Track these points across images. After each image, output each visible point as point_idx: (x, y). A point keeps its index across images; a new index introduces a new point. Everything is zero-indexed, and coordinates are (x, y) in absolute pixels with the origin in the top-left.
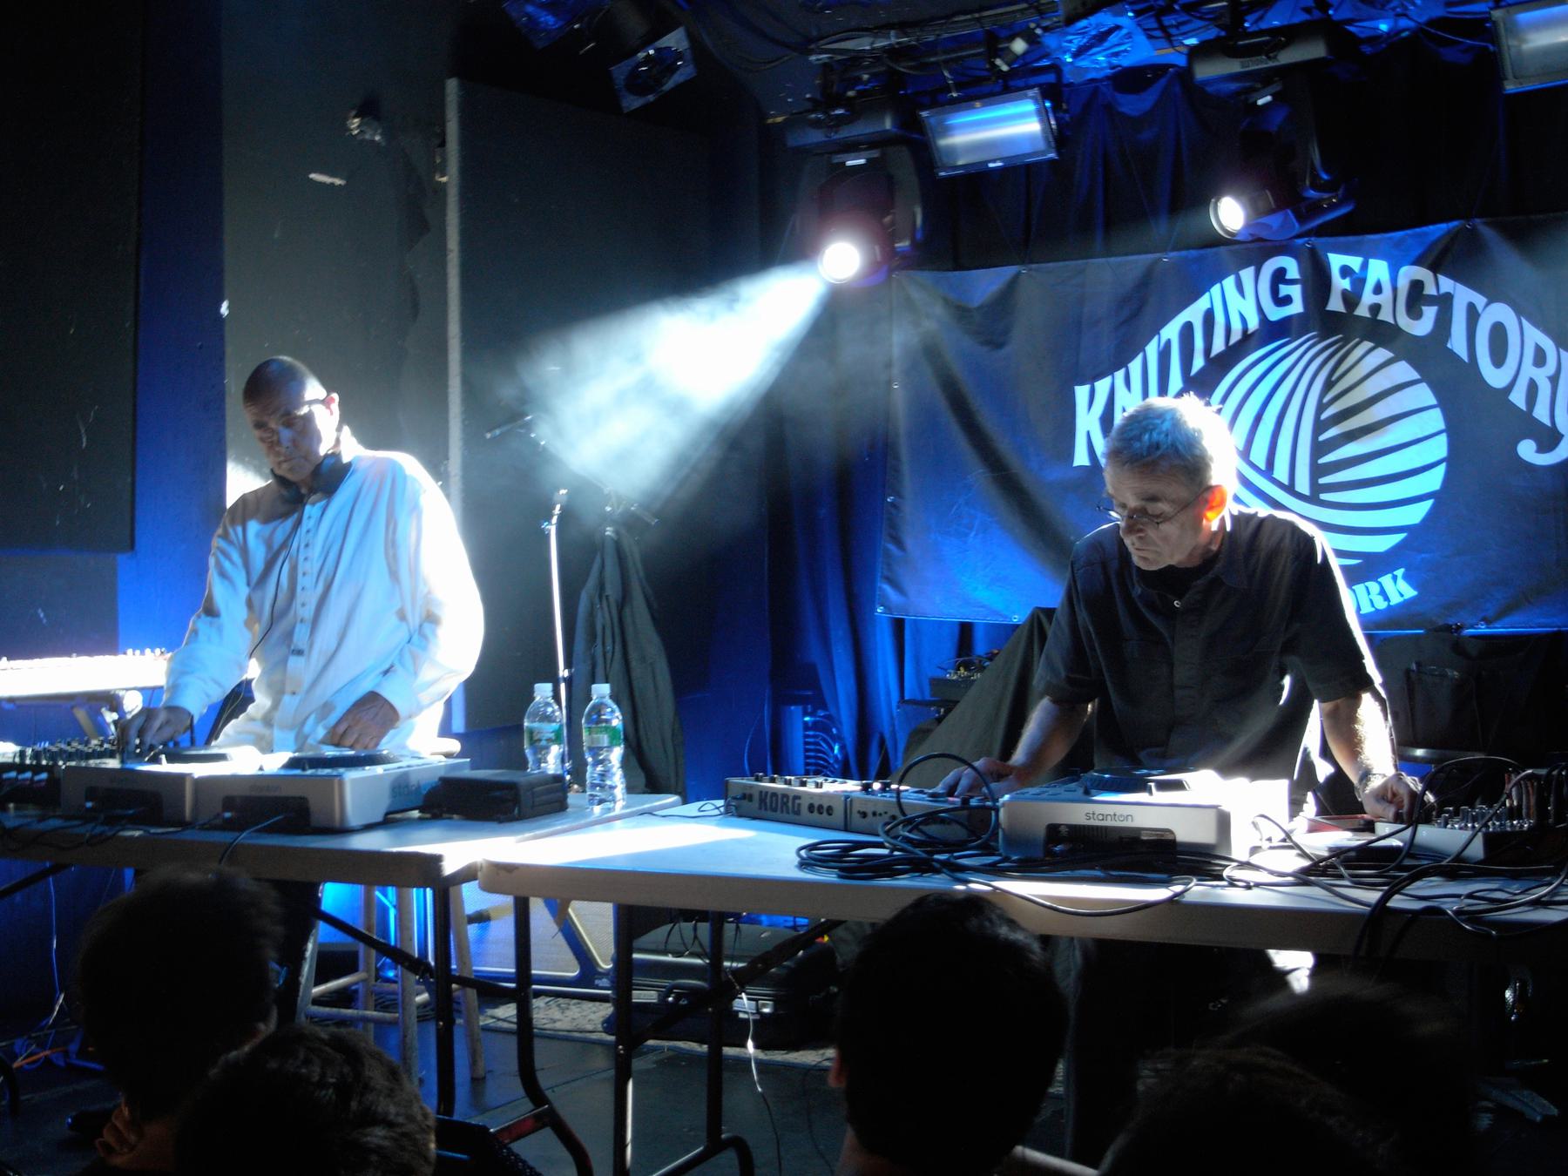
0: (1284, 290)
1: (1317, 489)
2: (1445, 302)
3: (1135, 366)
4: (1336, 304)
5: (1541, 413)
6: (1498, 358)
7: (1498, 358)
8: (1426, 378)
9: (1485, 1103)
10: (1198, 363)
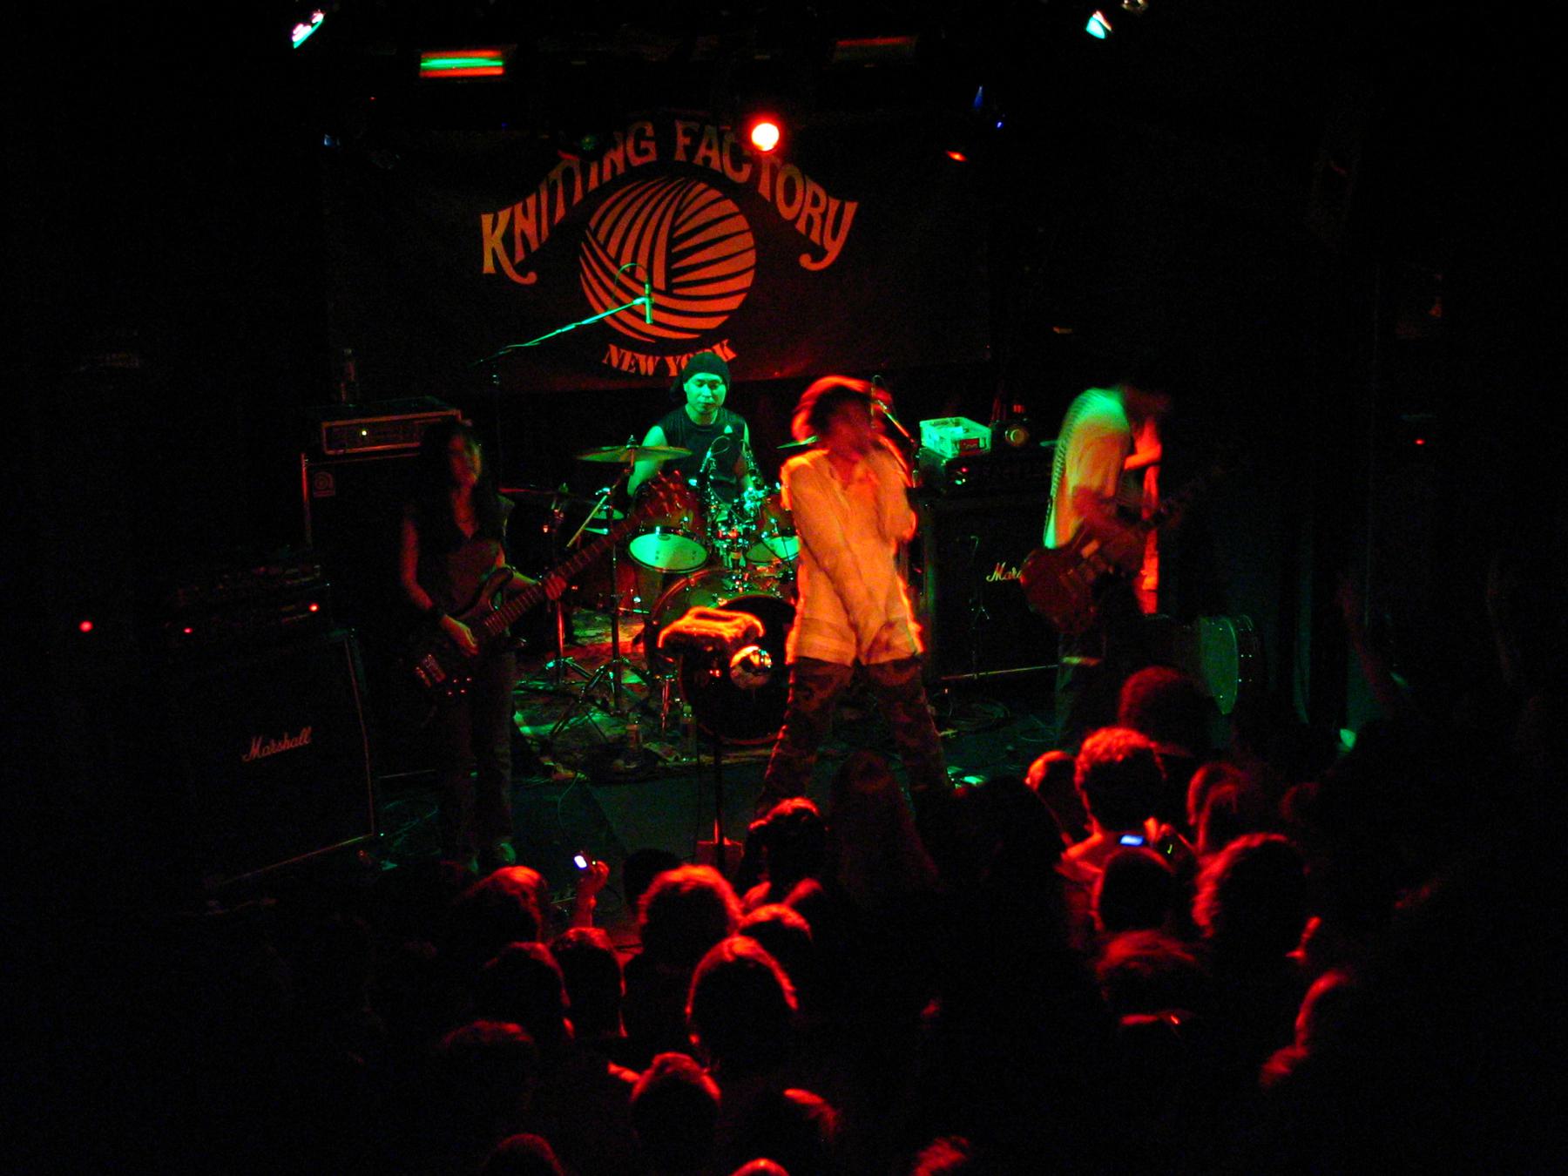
3: (531, 201)
4: (680, 156)
6: (789, 201)
7: (789, 201)
10: (578, 196)
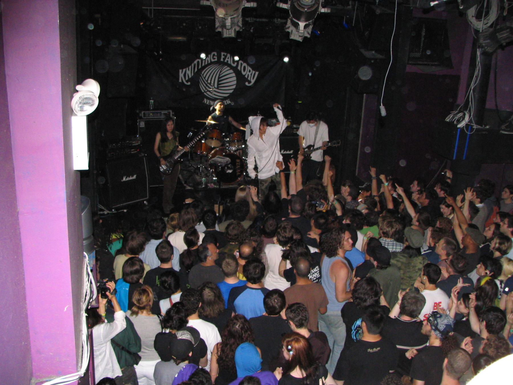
1: (218, 88)
3: (190, 67)
4: (222, 60)
5: (249, 79)
10: (200, 67)
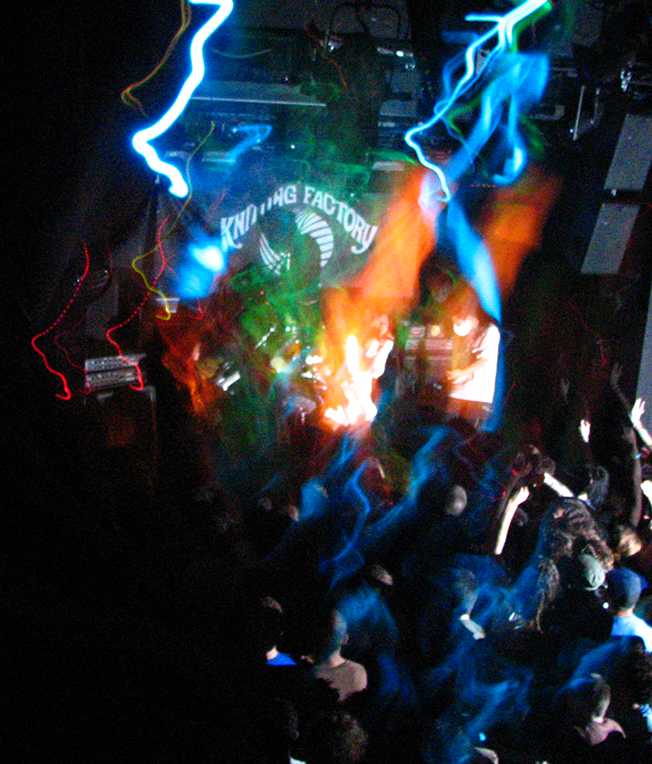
0: (292, 195)
2: (337, 206)
3: (243, 214)
4: (306, 201)
5: (358, 240)
8: (330, 226)
9: (615, 459)
